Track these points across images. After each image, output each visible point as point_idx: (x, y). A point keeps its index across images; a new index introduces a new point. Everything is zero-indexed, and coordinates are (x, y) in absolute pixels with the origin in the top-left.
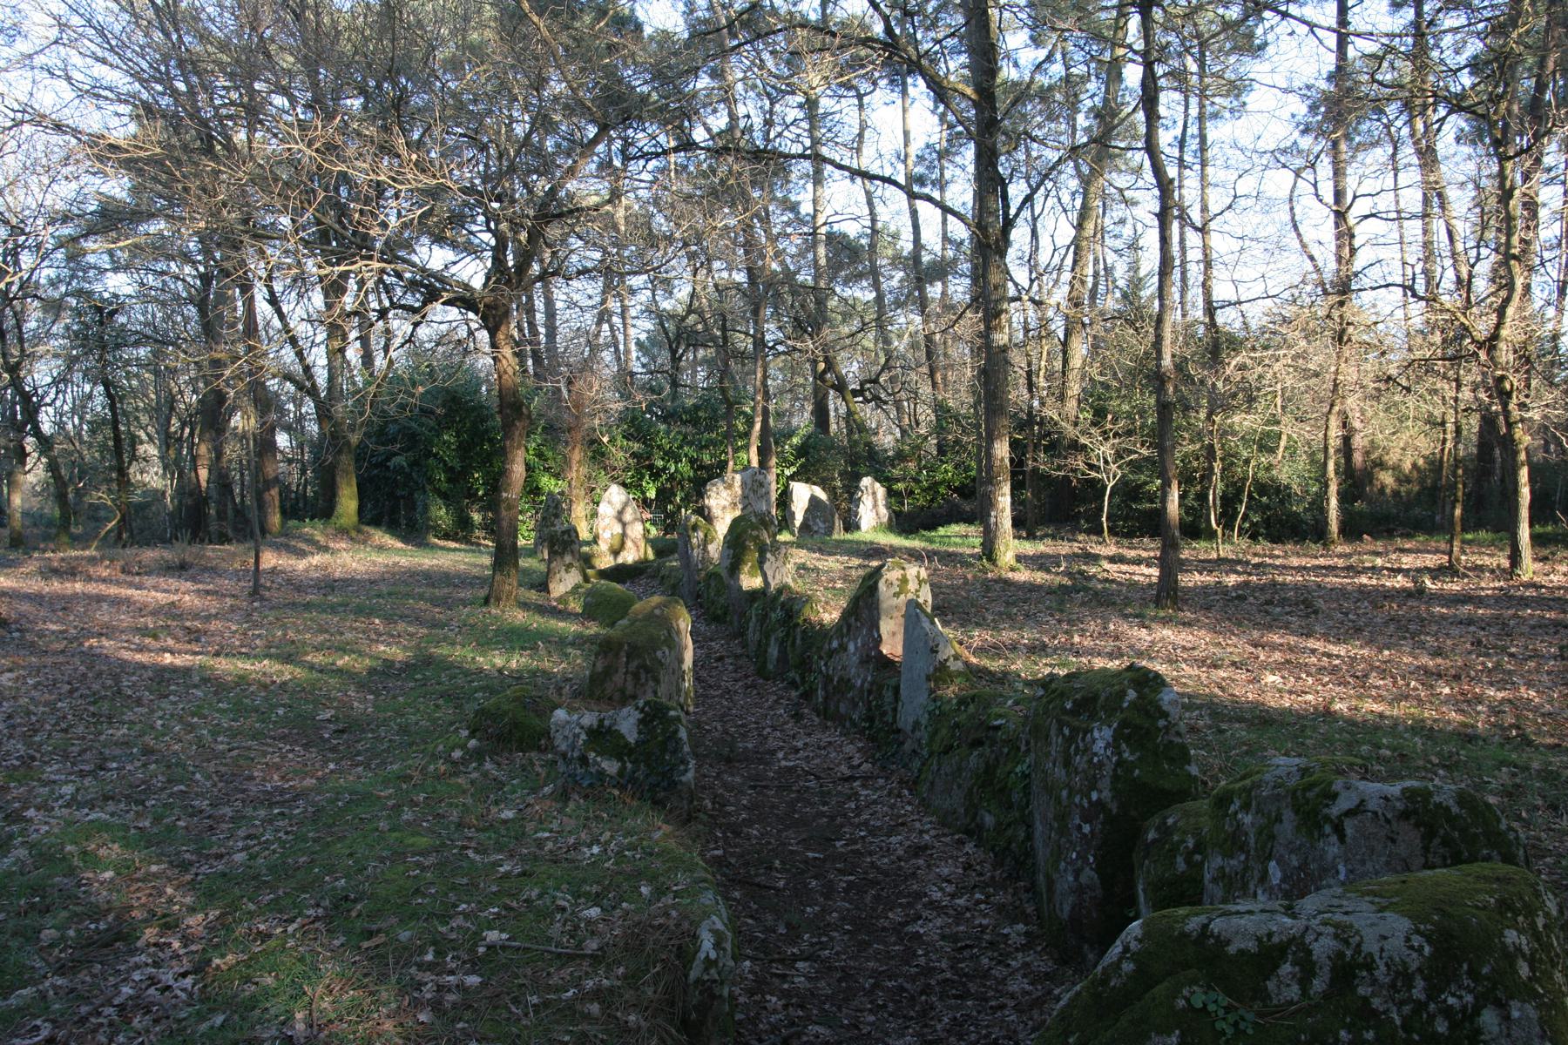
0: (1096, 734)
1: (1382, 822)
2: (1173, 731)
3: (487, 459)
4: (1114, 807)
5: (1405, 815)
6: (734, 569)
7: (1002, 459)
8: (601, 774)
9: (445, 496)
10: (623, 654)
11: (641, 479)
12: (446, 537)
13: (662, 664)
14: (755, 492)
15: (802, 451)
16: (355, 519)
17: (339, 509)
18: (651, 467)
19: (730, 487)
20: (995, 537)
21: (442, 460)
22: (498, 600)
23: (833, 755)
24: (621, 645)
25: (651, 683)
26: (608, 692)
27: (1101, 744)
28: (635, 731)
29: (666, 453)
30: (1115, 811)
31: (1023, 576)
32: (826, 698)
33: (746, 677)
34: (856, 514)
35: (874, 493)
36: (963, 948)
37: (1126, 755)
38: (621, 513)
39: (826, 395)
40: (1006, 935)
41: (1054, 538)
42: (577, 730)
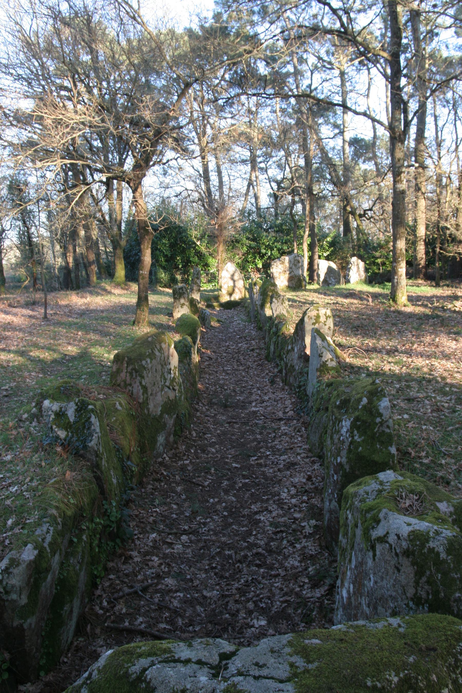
0: (344, 423)
1: (393, 554)
2: (385, 425)
3: (183, 251)
4: (347, 467)
5: (407, 553)
6: (263, 306)
7: (401, 250)
8: (58, 437)
9: (164, 268)
10: (125, 362)
11: (255, 259)
12: (165, 286)
13: (145, 368)
14: (295, 265)
15: (332, 244)
16: (124, 279)
17: (117, 274)
18: (259, 253)
19: (283, 263)
20: (397, 289)
21: (161, 251)
22: (139, 322)
23: (279, 405)
24: (123, 359)
25: (139, 378)
26: (118, 382)
27: (345, 429)
28: (74, 415)
29: (266, 246)
30: (348, 470)
31: (410, 309)
32: (286, 374)
33: (260, 360)
34: (348, 275)
35: (358, 265)
36: (278, 532)
37: (356, 438)
38: (233, 275)
39: (348, 217)
40: (304, 527)
41: (448, 286)
42: (50, 413)
